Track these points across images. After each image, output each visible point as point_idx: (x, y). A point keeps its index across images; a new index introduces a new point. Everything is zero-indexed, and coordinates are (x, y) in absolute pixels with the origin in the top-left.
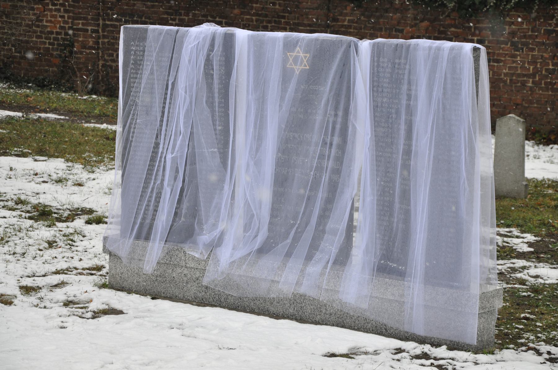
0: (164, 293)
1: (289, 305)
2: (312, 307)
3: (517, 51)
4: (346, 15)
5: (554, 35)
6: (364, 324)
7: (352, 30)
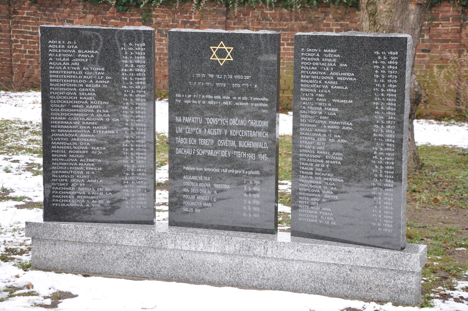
0: (92, 270)
1: (225, 273)
2: (249, 274)
3: (163, 36)
4: (25, 9)
5: (189, 25)
6: (303, 286)
7: (31, 21)
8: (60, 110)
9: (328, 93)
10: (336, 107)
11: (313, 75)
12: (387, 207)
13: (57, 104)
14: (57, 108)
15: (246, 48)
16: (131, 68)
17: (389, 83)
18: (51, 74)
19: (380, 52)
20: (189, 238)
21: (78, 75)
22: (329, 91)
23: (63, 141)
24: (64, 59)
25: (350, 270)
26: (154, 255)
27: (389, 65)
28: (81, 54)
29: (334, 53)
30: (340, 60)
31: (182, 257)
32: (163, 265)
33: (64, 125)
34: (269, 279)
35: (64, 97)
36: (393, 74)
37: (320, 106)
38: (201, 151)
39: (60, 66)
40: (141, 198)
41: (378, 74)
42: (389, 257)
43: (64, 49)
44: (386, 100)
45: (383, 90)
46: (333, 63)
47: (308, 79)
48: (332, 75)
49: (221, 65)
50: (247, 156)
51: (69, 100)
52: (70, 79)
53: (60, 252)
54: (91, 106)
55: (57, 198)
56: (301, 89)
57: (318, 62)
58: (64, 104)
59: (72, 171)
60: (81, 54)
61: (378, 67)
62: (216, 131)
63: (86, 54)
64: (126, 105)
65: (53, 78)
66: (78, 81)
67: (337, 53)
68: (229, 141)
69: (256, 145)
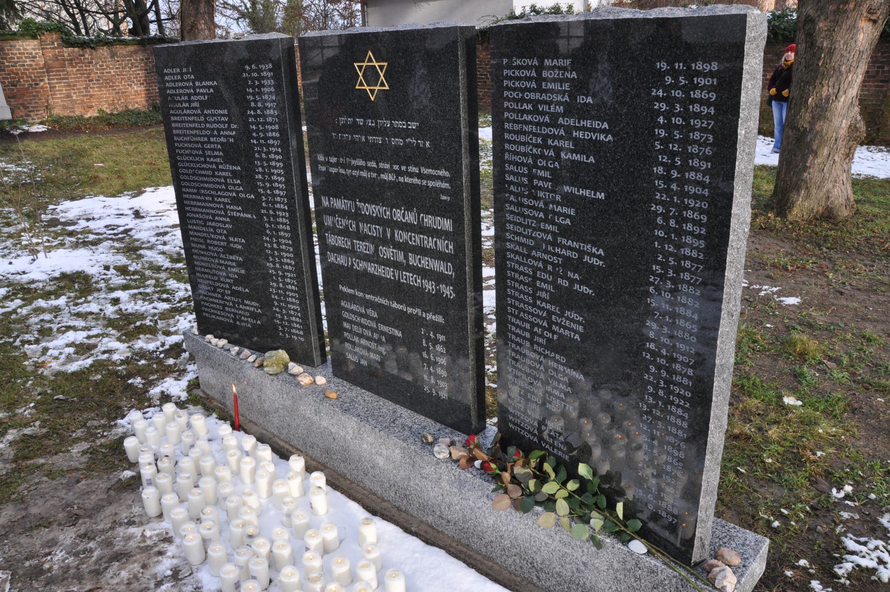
10: (572, 207)
17: (692, 156)
19: (671, 63)
27: (693, 101)
44: (683, 202)
45: (675, 174)
48: (561, 126)
61: (664, 107)
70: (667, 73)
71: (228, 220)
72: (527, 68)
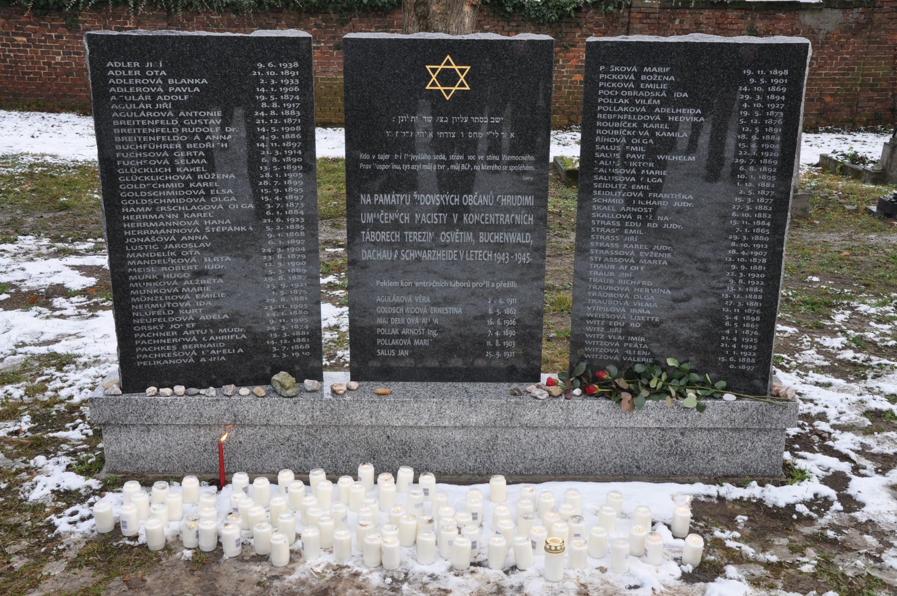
1: (466, 456)
2: (508, 454)
8: (139, 194)
9: (649, 144)
11: (621, 113)
12: (747, 332)
13: (131, 182)
14: (134, 190)
15: (494, 67)
16: (273, 109)
17: (768, 126)
18: (117, 127)
19: (754, 71)
20: (402, 406)
21: (171, 127)
22: (651, 141)
23: (149, 251)
24: (141, 97)
25: (682, 434)
26: (337, 436)
28: (175, 86)
29: (665, 74)
30: (673, 87)
31: (388, 437)
32: (354, 451)
33: (148, 221)
34: (543, 460)
35: (145, 170)
36: (776, 110)
37: (632, 168)
38: (408, 254)
39: (133, 110)
40: (298, 340)
41: (747, 109)
42: (750, 410)
43: (138, 77)
46: (661, 91)
47: (611, 121)
48: (657, 113)
49: (448, 98)
50: (493, 257)
51: (155, 175)
52: (156, 134)
53: (158, 442)
54: (199, 184)
55: (144, 352)
56: (597, 139)
57: (632, 89)
58: (145, 183)
59: (169, 304)
60: (175, 86)
62: (438, 217)
63: (184, 85)
64: (265, 179)
65: (121, 135)
66: (172, 138)
67: (669, 74)
68: (461, 233)
69: (513, 238)
70: (751, 76)
71: (205, 237)
72: (626, 73)
